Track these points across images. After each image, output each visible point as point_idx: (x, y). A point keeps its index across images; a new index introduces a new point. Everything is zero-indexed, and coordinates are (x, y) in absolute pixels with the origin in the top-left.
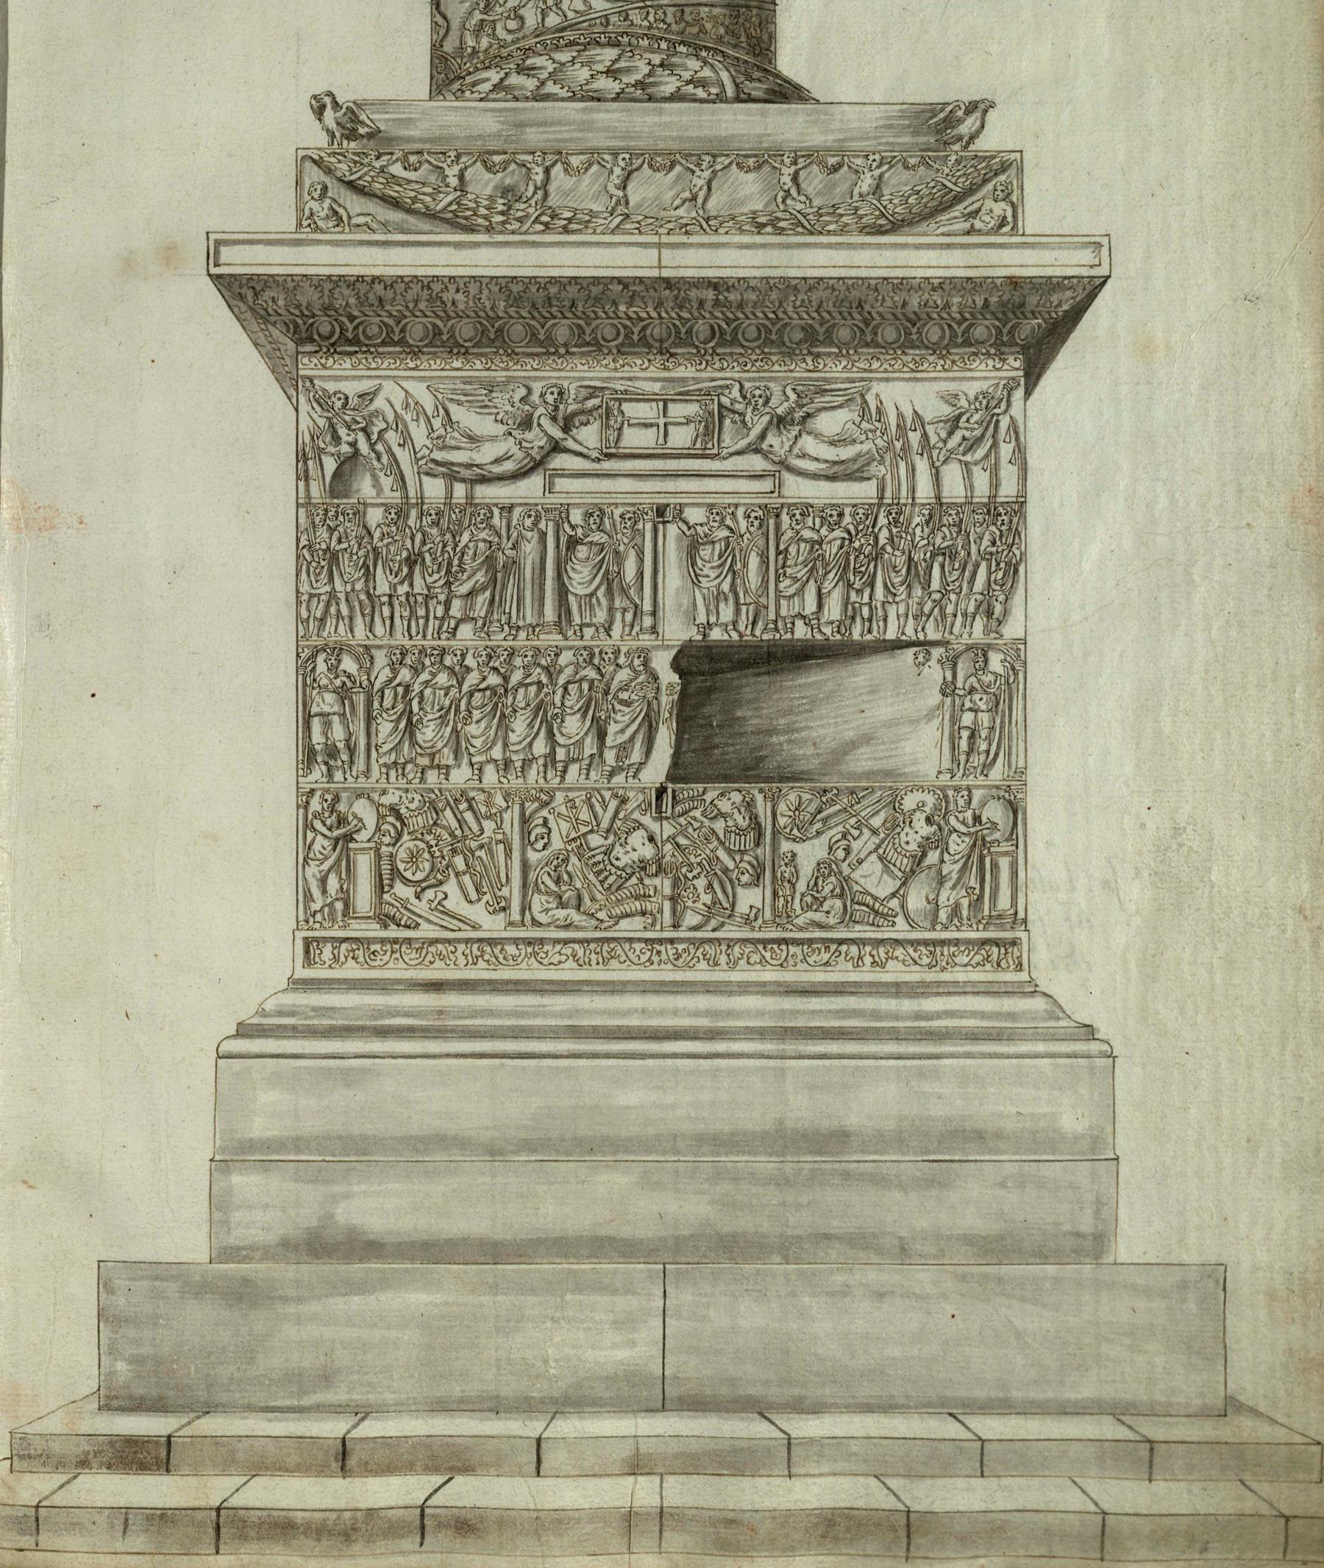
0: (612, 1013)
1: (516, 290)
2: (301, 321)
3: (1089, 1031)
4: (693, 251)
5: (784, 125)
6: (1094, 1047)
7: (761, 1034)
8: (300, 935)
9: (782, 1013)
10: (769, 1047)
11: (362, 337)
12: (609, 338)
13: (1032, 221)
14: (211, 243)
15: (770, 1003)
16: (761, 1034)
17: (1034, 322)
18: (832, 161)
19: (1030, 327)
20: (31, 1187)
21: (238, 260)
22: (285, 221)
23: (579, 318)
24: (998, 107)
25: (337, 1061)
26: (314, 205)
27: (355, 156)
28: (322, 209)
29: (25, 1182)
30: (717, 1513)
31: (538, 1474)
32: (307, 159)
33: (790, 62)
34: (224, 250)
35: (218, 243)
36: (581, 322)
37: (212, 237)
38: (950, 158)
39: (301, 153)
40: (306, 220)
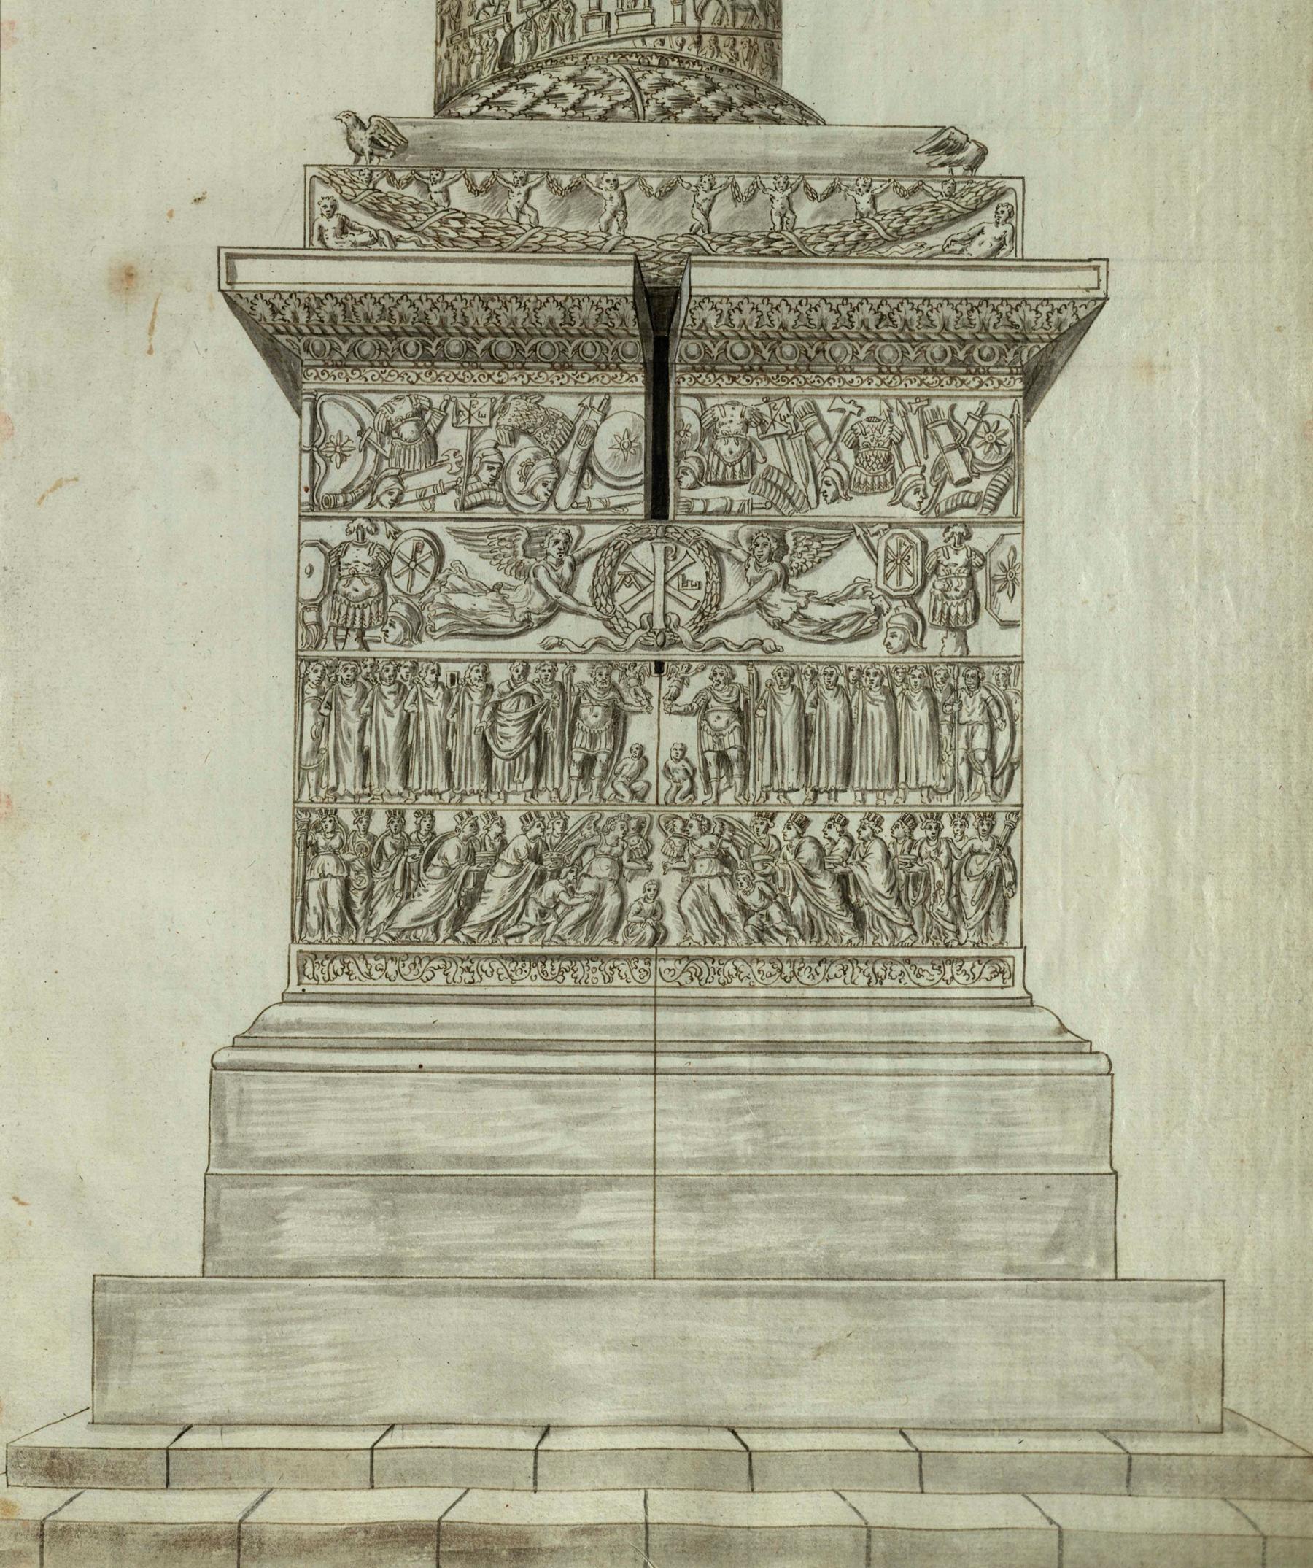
3: (1082, 1047)
4: (1037, 274)
5: (785, 144)
6: (1089, 1063)
7: (750, 1048)
8: (295, 948)
9: (894, 1028)
10: (759, 1062)
11: (948, 360)
12: (739, 355)
14: (223, 257)
15: (759, 1017)
16: (750, 1048)
20: (23, 1204)
21: (253, 275)
22: (294, 236)
23: (561, 336)
25: (730, 1077)
26: (323, 221)
27: (380, 172)
28: (331, 224)
29: (16, 1199)
30: (326, 1529)
31: (373, 1487)
32: (329, 175)
33: (793, 81)
34: (241, 265)
36: (563, 340)
37: (1103, 264)
38: (952, 181)
39: (312, 171)
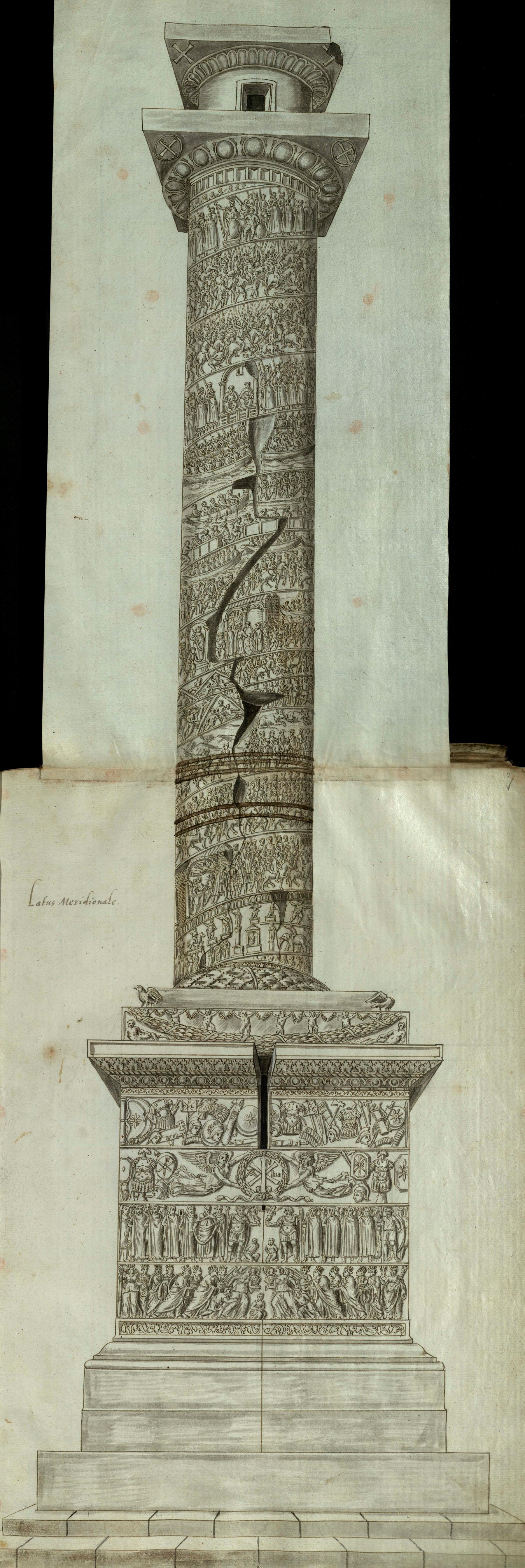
0: (208, 1352)
1: (156, 1062)
2: (118, 1077)
3: (432, 1360)
5: (314, 998)
6: (435, 1366)
7: (300, 1360)
9: (358, 1352)
13: (413, 1039)
17: (414, 1081)
18: (363, 1015)
19: (411, 1082)
21: (101, 1051)
22: (118, 1036)
24: (137, 983)
26: (129, 1029)
32: (132, 1011)
33: (317, 974)
35: (92, 1043)
38: (380, 1013)
39: (124, 1009)
40: (126, 1035)
